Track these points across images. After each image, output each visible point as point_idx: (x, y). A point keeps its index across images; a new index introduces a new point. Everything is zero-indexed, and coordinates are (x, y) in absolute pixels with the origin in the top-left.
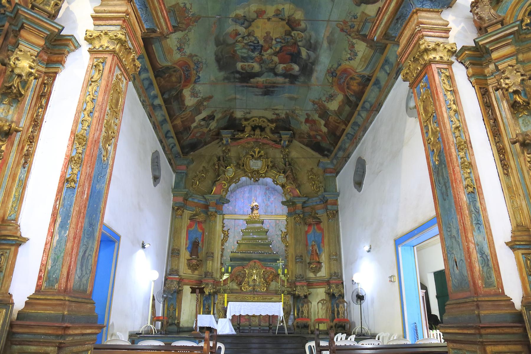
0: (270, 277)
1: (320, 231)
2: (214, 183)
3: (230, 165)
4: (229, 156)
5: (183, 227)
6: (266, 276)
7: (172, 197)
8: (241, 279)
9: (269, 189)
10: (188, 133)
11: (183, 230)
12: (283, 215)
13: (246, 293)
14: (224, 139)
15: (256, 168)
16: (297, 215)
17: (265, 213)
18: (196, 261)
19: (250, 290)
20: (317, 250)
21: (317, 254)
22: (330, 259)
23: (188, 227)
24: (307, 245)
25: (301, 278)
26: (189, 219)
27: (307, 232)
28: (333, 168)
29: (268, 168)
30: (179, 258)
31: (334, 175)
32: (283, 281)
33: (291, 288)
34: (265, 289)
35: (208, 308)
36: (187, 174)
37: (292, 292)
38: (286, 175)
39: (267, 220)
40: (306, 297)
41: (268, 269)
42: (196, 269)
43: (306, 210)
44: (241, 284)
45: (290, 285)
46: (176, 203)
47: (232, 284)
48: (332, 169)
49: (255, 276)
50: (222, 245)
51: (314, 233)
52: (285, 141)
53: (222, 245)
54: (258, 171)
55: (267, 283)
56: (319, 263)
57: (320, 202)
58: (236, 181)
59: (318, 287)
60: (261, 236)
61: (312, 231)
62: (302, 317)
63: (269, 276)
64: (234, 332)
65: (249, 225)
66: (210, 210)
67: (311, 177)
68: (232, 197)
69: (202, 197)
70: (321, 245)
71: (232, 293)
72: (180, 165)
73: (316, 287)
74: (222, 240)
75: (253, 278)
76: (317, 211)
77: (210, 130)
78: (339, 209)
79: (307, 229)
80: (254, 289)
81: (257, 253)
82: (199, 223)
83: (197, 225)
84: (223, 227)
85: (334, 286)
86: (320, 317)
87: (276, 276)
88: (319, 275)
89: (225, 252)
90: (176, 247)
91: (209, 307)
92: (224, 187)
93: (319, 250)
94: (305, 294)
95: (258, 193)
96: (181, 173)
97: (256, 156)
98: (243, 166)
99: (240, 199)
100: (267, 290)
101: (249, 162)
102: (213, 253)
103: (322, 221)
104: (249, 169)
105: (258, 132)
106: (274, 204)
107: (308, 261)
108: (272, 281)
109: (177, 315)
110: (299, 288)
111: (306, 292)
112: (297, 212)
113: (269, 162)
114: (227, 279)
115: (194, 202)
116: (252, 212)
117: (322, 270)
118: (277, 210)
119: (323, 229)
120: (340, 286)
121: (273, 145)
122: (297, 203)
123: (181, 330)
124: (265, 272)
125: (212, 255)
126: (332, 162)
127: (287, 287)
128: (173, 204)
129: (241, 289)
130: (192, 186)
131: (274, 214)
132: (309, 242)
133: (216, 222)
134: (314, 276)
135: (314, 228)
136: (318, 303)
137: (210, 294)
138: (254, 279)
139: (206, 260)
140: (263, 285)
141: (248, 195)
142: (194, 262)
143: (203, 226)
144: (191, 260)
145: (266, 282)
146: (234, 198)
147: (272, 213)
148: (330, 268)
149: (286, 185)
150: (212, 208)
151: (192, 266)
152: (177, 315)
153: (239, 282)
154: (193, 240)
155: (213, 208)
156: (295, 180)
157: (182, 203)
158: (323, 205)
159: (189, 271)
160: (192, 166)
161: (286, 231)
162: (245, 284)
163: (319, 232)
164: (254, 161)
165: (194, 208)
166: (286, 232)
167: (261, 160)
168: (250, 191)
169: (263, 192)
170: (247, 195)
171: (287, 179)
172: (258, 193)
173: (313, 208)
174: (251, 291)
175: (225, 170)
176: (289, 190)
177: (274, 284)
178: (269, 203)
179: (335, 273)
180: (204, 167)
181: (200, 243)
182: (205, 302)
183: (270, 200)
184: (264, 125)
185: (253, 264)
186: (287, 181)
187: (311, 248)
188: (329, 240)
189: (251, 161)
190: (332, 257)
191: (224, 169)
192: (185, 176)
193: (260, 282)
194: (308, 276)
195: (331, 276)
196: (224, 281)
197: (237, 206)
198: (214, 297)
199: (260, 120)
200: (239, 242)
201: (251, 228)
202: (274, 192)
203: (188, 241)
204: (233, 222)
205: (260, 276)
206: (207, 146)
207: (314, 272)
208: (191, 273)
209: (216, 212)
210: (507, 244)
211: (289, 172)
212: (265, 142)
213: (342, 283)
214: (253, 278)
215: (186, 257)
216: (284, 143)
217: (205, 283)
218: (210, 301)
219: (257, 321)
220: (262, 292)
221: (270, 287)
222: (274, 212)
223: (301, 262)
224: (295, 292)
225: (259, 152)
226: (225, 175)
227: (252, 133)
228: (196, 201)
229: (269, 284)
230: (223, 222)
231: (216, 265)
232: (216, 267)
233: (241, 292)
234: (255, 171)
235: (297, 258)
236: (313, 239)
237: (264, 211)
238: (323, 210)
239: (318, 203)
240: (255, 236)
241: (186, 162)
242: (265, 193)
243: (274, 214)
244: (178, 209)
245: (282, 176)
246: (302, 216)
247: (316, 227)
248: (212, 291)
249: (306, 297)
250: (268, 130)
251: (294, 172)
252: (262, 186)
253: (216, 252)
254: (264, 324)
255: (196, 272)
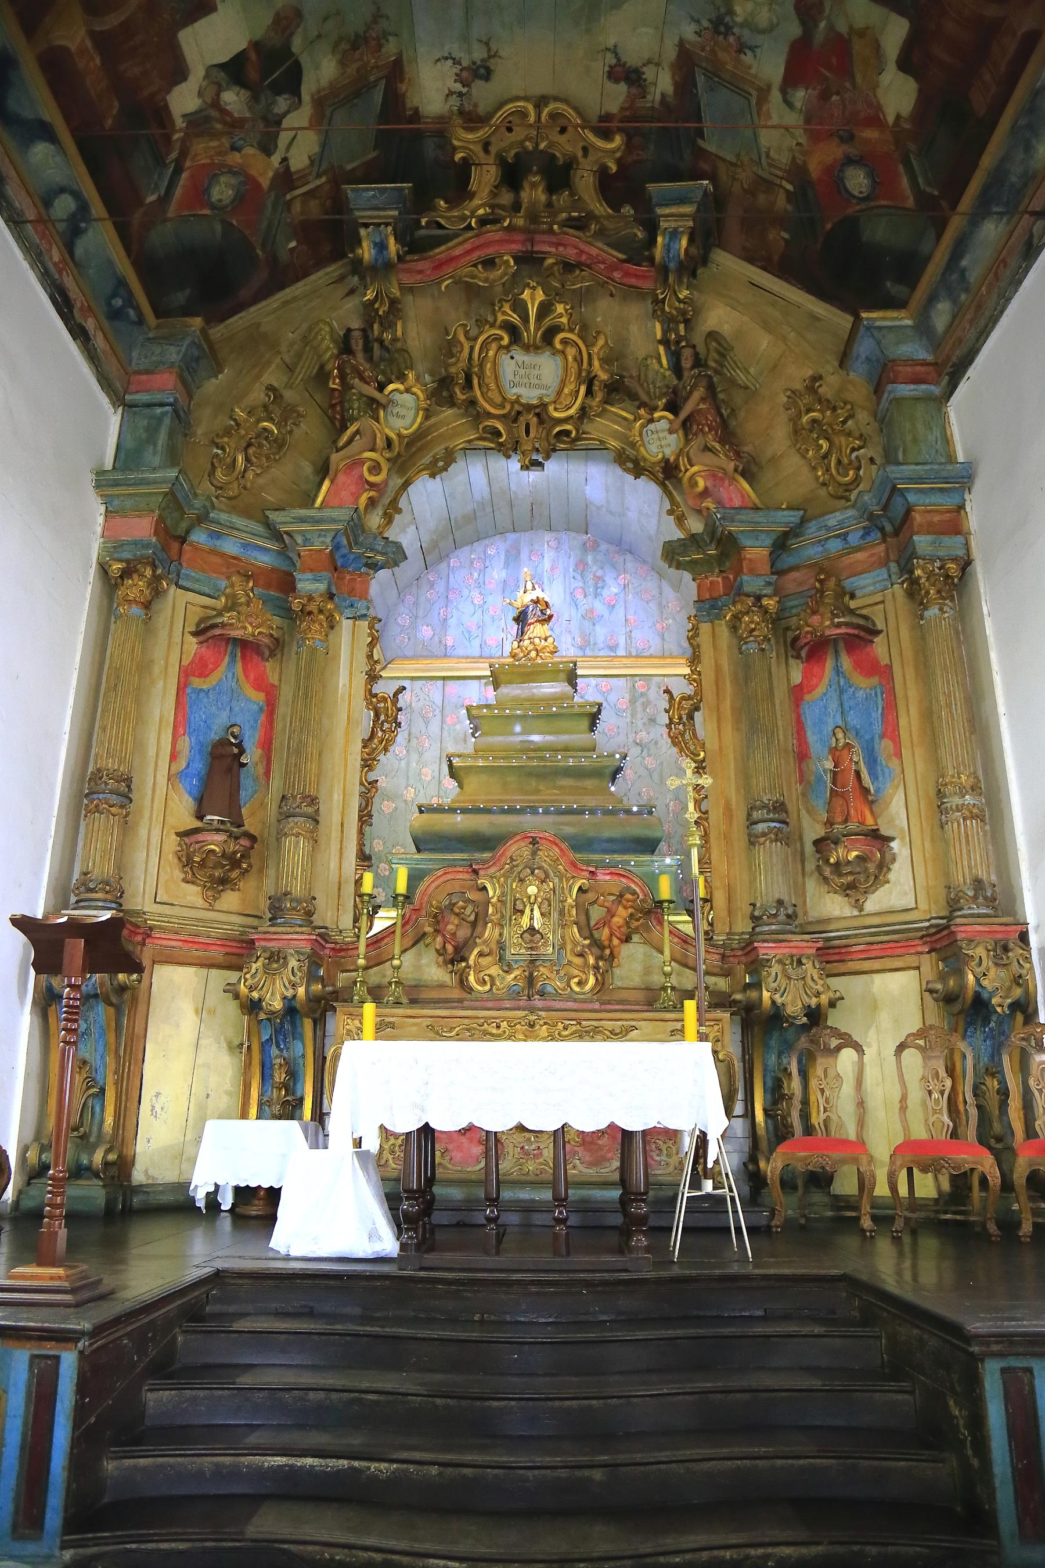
0: (617, 920)
1: (875, 680)
2: (323, 470)
3: (401, 378)
4: (395, 340)
5: (157, 670)
6: (597, 913)
7: (101, 519)
8: (463, 933)
9: (595, 547)
10: (160, 161)
11: (160, 684)
12: (663, 657)
13: (493, 1001)
14: (363, 232)
15: (530, 396)
16: (750, 601)
17: (581, 648)
18: (221, 837)
19: (510, 988)
20: (865, 775)
21: (866, 791)
22: (942, 810)
23: (186, 674)
24: (802, 755)
25: (782, 917)
26: (195, 634)
27: (798, 693)
28: (930, 358)
29: (589, 392)
30: (127, 826)
31: (936, 390)
32: (685, 940)
33: (726, 974)
34: (592, 981)
35: (285, 1085)
36: (182, 419)
37: (738, 997)
38: (683, 414)
39: (593, 681)
40: (815, 1016)
41: (602, 877)
42: (224, 882)
43: (792, 582)
44: (464, 959)
45: (723, 957)
46: (119, 546)
47: (419, 955)
48: (924, 363)
49: (537, 913)
50: (368, 764)
51: (842, 692)
52: (674, 234)
53: (368, 764)
54: (540, 411)
55: (602, 948)
56: (879, 838)
57: (867, 531)
58: (435, 461)
59: (876, 965)
60: (565, 738)
61: (826, 680)
62: (809, 1130)
63: (611, 914)
64: (388, 1244)
65: (504, 690)
66: (300, 586)
67: (814, 421)
68: (432, 585)
69: (260, 529)
70: (884, 747)
71: (413, 1002)
72: (148, 372)
73: (867, 965)
74: (366, 743)
75: (525, 921)
76: (849, 583)
77: (286, 179)
78: (976, 553)
79: (797, 677)
80: (531, 980)
81: (546, 812)
82: (246, 647)
83: (239, 666)
84: (373, 677)
85: (980, 951)
86: (920, 1133)
87: (649, 912)
88: (874, 902)
89: (382, 807)
90: (111, 764)
91: (293, 1075)
92: (372, 479)
93: (873, 775)
94: (814, 1002)
95: (547, 564)
96: (149, 405)
97: (532, 331)
98: (468, 384)
99: (466, 592)
100: (601, 985)
101: (494, 363)
102: (313, 801)
103: (880, 626)
104: (498, 400)
105: (534, 192)
106: (620, 611)
107: (813, 830)
108: (627, 939)
109: (109, 1120)
110: (776, 968)
111: (818, 994)
112: (747, 589)
113: (596, 363)
114: (389, 932)
115: (222, 555)
116: (522, 633)
117: (891, 876)
118: (637, 635)
119: (889, 667)
120: (1016, 952)
121: (612, 268)
122: (745, 541)
123: (137, 1200)
124: (591, 896)
125: (310, 810)
126: (923, 328)
127: (707, 973)
128: (103, 549)
129: (463, 983)
130: (212, 473)
131: (621, 652)
132: (811, 738)
133: (330, 655)
134: (848, 911)
135: (838, 671)
136: (901, 1048)
137: (291, 1010)
138: (532, 930)
139: (281, 835)
140: (578, 961)
141: (504, 574)
142: (215, 842)
143: (271, 670)
144: (196, 831)
145: (596, 944)
146: (440, 586)
147: (613, 648)
148: (942, 862)
149: (683, 462)
150: (309, 576)
151: (203, 864)
152: (109, 1120)
153: (450, 948)
154: (215, 736)
155: (316, 580)
156: (728, 436)
157: (148, 546)
158: (882, 548)
159: (193, 894)
160: (212, 386)
161: (690, 690)
162: (481, 954)
163: (864, 685)
164: (520, 355)
165: (223, 583)
166: (689, 698)
167: (555, 352)
168: (513, 558)
169: (572, 562)
170: (497, 573)
171: (686, 435)
172: (547, 564)
173: (824, 570)
174: (514, 994)
175: (376, 395)
176: (701, 484)
177: (640, 956)
178: (599, 607)
179: (978, 883)
180: (270, 388)
181: (252, 756)
182: (274, 1051)
183: (605, 593)
184: (564, 146)
185: (526, 852)
186: (687, 441)
187: (829, 765)
188: (929, 716)
189: (504, 358)
190: (957, 801)
191: (371, 391)
192: (167, 421)
193: (563, 947)
194: (813, 914)
195: (953, 905)
196: (376, 942)
197: (452, 622)
198: (320, 1022)
199: (545, 112)
200: (456, 761)
201: (518, 702)
202: (620, 559)
203: (185, 744)
204: (435, 691)
205: (562, 913)
206: (288, 293)
207: (848, 889)
208: (200, 902)
209: (331, 596)
210: (427, 1123)
211: (697, 395)
212: (571, 254)
213: (1024, 937)
214: (525, 921)
215: (170, 820)
216: (667, 248)
217: (265, 949)
218: (298, 1045)
219: (548, 1154)
220: (572, 997)
221: (617, 971)
222: (622, 641)
223: (779, 837)
224: (753, 994)
225: (545, 310)
226: (377, 420)
227: (506, 198)
228: (230, 547)
229: (612, 956)
230: (370, 656)
231: (333, 864)
232: (334, 876)
233: (461, 1001)
234: (529, 407)
235: (756, 815)
236: (834, 719)
237: (578, 639)
238: (883, 573)
239: (854, 539)
240: (536, 738)
241: (173, 354)
242: (581, 566)
243: (621, 652)
244: (126, 574)
245: (663, 425)
246: (770, 603)
247: (846, 662)
248: (301, 991)
249: (815, 1016)
250: (585, 181)
251: (721, 396)
252: (563, 536)
253: (337, 797)
254: (590, 1173)
255: (230, 900)
